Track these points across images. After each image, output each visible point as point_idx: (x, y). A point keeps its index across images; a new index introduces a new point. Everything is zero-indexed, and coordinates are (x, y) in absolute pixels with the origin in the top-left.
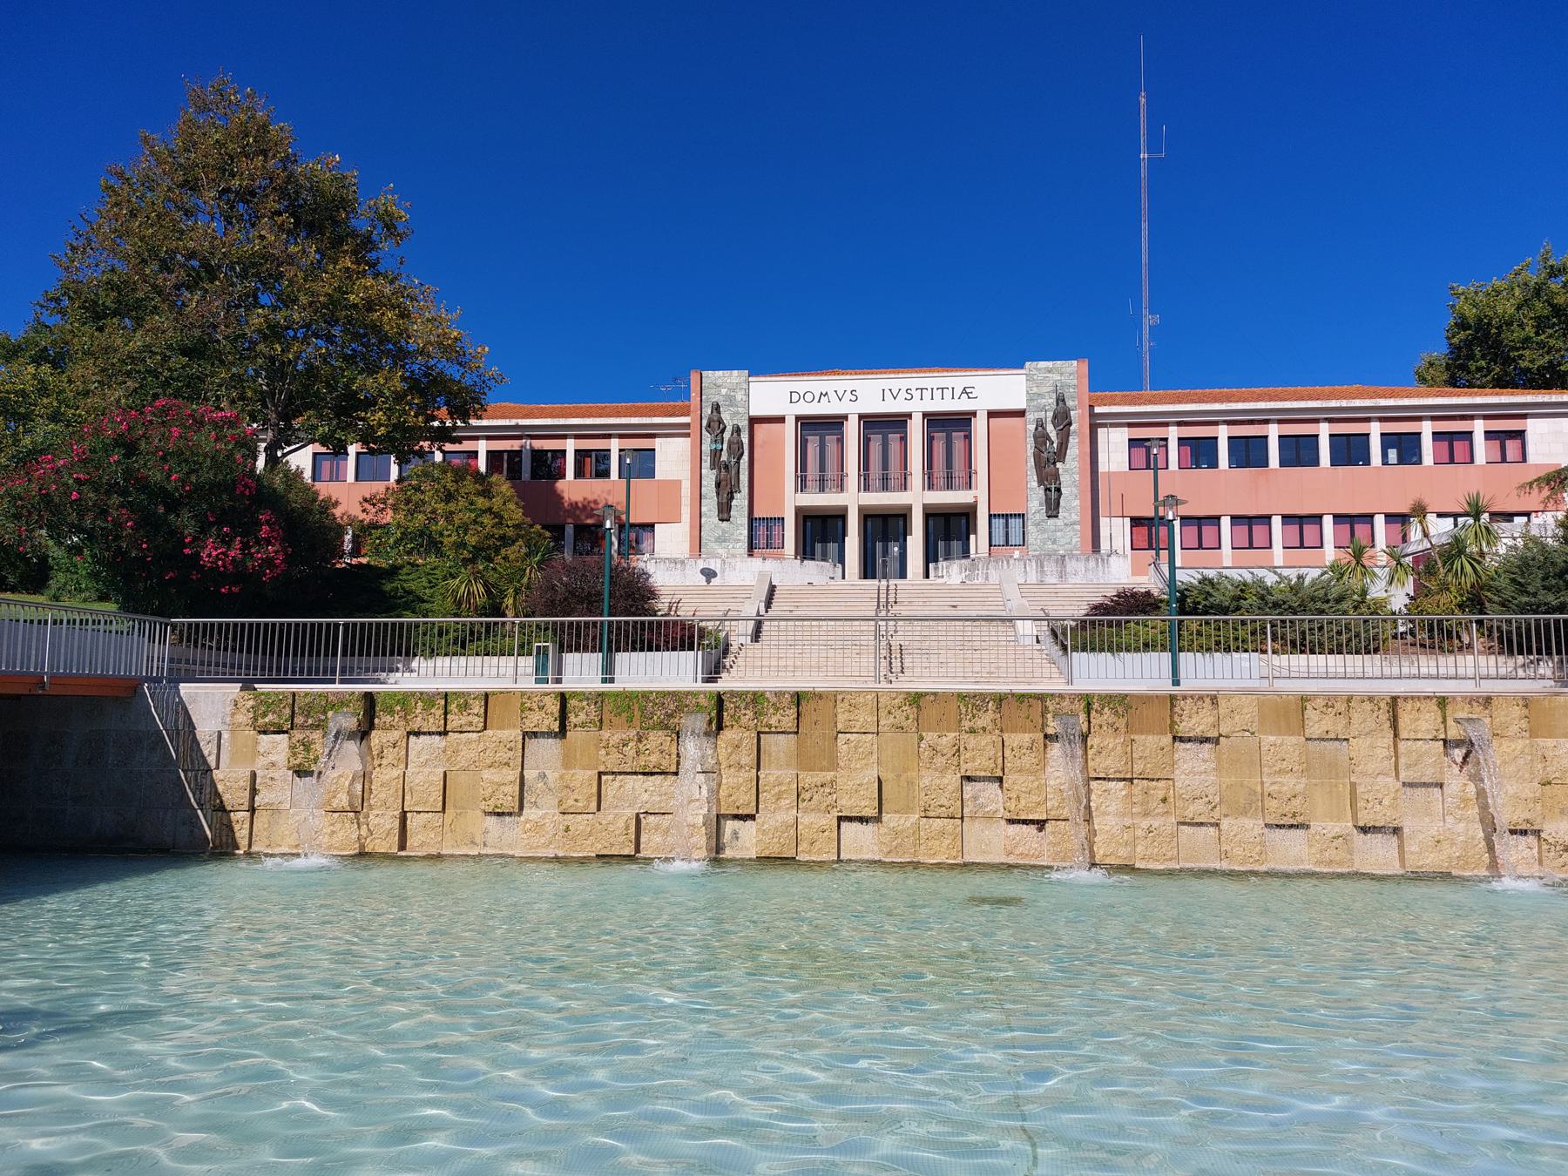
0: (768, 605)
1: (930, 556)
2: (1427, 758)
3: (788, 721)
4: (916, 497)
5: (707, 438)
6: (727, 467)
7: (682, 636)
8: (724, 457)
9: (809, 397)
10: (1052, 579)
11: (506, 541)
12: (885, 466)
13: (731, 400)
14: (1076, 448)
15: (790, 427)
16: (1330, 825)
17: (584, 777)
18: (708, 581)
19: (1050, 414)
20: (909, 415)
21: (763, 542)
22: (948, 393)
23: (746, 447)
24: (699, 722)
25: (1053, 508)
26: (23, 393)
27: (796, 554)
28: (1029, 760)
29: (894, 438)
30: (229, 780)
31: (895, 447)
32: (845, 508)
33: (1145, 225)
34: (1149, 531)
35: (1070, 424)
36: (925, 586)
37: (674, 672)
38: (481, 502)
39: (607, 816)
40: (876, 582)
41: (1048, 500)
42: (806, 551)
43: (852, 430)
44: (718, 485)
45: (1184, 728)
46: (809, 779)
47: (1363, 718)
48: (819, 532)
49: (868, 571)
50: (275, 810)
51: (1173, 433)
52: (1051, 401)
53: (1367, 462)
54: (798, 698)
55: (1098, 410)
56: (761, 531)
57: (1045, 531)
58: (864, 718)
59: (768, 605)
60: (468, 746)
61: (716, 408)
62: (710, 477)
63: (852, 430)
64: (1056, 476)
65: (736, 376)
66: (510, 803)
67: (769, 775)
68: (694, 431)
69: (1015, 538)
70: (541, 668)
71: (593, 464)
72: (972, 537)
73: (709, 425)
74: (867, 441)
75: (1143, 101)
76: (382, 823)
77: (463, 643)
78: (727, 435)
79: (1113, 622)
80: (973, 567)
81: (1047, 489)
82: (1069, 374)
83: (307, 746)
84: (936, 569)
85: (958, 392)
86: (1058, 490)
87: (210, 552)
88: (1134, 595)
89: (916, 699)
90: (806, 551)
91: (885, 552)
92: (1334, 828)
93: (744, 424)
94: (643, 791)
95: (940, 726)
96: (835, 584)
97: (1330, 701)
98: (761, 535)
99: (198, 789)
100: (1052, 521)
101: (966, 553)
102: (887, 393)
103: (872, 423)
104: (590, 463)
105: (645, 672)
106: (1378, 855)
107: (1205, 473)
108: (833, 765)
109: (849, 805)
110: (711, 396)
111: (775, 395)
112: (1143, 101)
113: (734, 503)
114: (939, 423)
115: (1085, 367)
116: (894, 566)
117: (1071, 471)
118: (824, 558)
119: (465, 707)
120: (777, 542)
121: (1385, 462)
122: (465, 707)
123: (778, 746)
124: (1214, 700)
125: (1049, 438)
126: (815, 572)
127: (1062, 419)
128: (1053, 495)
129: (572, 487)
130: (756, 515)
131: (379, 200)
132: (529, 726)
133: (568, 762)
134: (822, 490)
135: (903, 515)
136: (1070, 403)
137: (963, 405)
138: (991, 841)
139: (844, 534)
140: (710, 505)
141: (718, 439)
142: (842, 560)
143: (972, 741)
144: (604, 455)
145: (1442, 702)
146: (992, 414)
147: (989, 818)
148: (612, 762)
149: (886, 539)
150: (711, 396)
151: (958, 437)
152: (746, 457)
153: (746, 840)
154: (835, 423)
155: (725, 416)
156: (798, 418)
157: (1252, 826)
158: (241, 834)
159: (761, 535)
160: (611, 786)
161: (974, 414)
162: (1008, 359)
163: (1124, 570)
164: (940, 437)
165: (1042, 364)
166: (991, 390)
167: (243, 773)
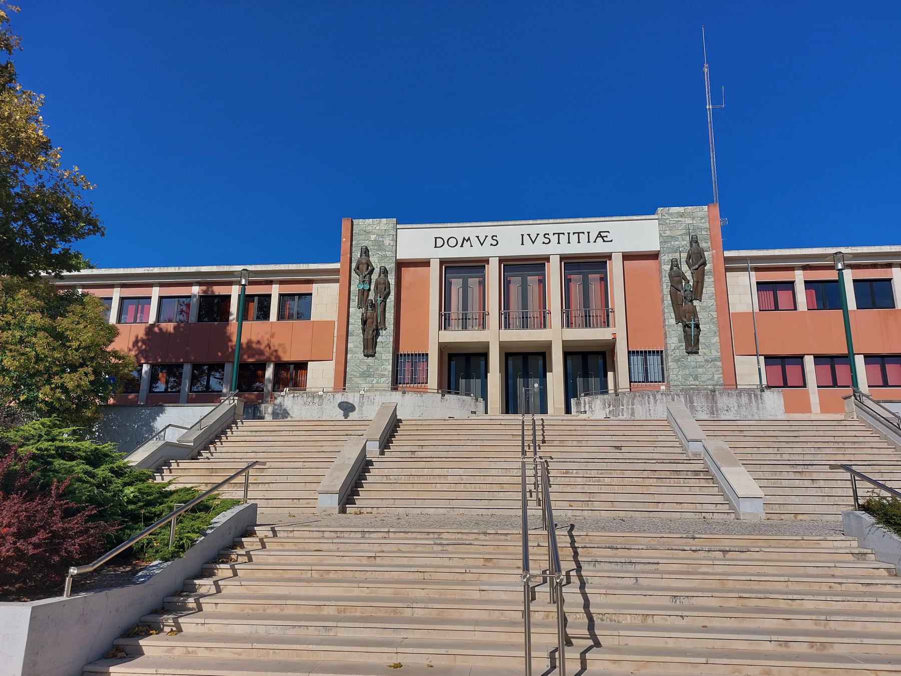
1: (570, 392)
4: (556, 335)
5: (356, 278)
6: (373, 306)
8: (372, 296)
9: (452, 242)
12: (525, 305)
13: (380, 245)
15: (434, 269)
18: (346, 416)
19: (684, 255)
20: (547, 259)
21: (408, 376)
22: (583, 238)
23: (392, 287)
25: (692, 345)
27: (440, 386)
29: (594, 278)
31: (595, 287)
32: (486, 345)
35: (704, 264)
36: (579, 425)
40: (519, 417)
41: (687, 337)
42: (448, 386)
43: (493, 272)
44: (364, 322)
48: (462, 368)
49: (510, 405)
52: (685, 242)
57: (685, 367)
61: (366, 252)
62: (356, 314)
63: (493, 272)
64: (694, 313)
72: (610, 375)
73: (358, 267)
78: (375, 276)
81: (686, 326)
82: (701, 219)
84: (578, 404)
85: (593, 237)
86: (697, 326)
90: (448, 386)
91: (526, 385)
93: (391, 266)
96: (478, 416)
100: (691, 358)
102: (526, 238)
103: (510, 265)
104: (131, 308)
111: (417, 241)
113: (379, 339)
114: (574, 264)
116: (535, 401)
117: (706, 309)
120: (421, 376)
125: (685, 278)
126: (456, 406)
127: (697, 259)
130: (401, 351)
134: (465, 328)
136: (703, 245)
137: (599, 248)
139: (487, 371)
140: (356, 342)
144: (837, 285)
146: (627, 257)
149: (526, 375)
150: (360, 241)
152: (392, 297)
154: (477, 266)
155: (374, 260)
156: (442, 262)
159: (405, 372)
162: (645, 208)
164: (576, 278)
165: (674, 210)
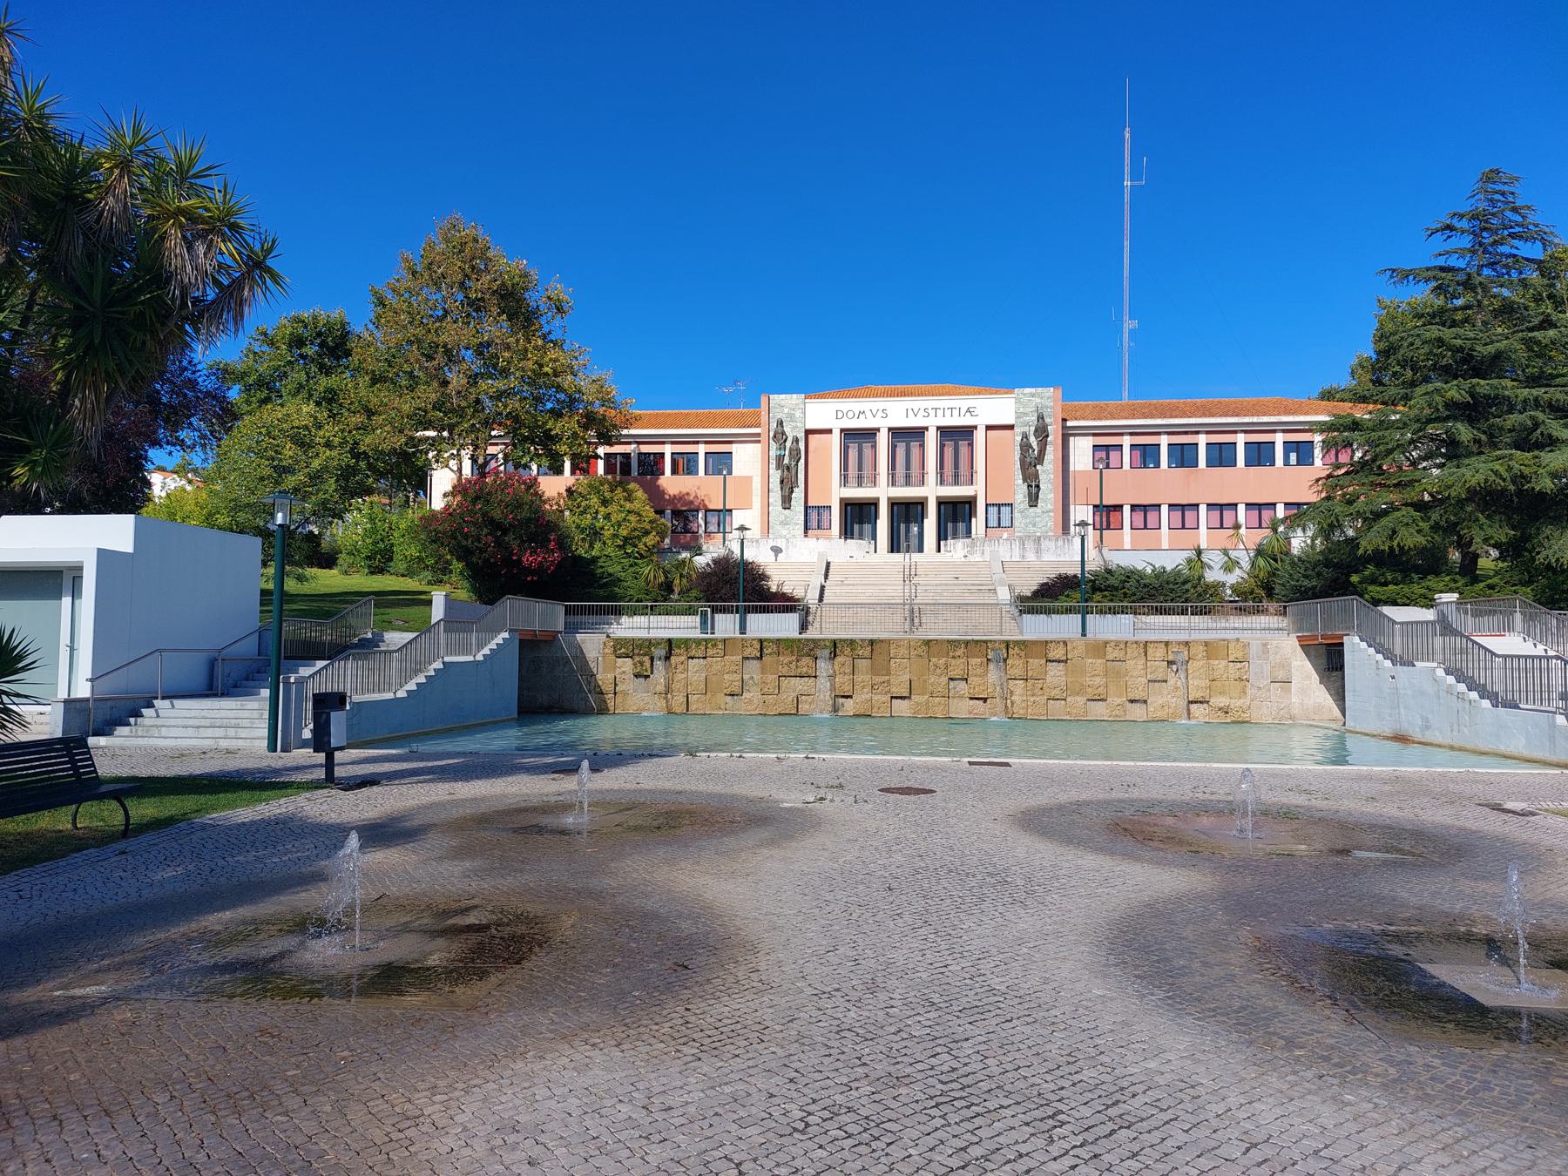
0: (826, 577)
1: (942, 536)
2: (1160, 670)
3: (867, 653)
4: (931, 491)
7: (784, 603)
8: (786, 461)
10: (1031, 556)
11: (647, 533)
13: (791, 417)
14: (1053, 454)
15: (836, 437)
16: (1115, 700)
17: (771, 678)
22: (956, 412)
24: (826, 652)
25: (1033, 500)
26: (306, 427)
28: (979, 671)
29: (915, 445)
30: (604, 678)
31: (915, 451)
33: (1127, 243)
36: (942, 562)
37: (783, 626)
38: (628, 506)
40: (901, 555)
41: (1030, 494)
42: (847, 533)
45: (1051, 656)
48: (857, 516)
49: (894, 547)
50: (625, 694)
51: (1126, 441)
53: (1273, 464)
54: (872, 642)
55: (1069, 424)
56: (814, 516)
58: (903, 651)
59: (826, 577)
60: (716, 663)
61: (781, 423)
62: (776, 476)
63: (883, 439)
64: (1037, 476)
65: (794, 399)
67: (858, 678)
68: (764, 438)
69: (1005, 521)
70: (704, 622)
71: (685, 465)
74: (894, 447)
75: (1127, 135)
78: (788, 444)
79: (1054, 594)
80: (973, 545)
83: (642, 663)
87: (527, 559)
88: (1067, 577)
89: (928, 643)
90: (847, 533)
91: (908, 530)
92: (1119, 701)
93: (801, 435)
94: (800, 685)
95: (939, 656)
97: (1117, 644)
98: (813, 520)
101: (968, 533)
103: (898, 434)
105: (765, 625)
106: (1137, 712)
107: (1150, 472)
108: (888, 674)
109: (896, 691)
110: (777, 414)
111: (826, 413)
112: (1127, 135)
115: (1059, 393)
116: (914, 542)
117: (1048, 472)
118: (861, 537)
119: (715, 645)
120: (825, 524)
121: (1287, 463)
122: (715, 645)
123: (863, 664)
124: (1065, 643)
127: (1042, 432)
128: (1034, 490)
129: (671, 483)
131: (546, 287)
132: (746, 654)
133: (763, 671)
134: (860, 485)
135: (921, 504)
136: (1047, 420)
137: (966, 421)
138: (962, 708)
140: (776, 497)
141: (782, 446)
142: (874, 537)
143: (953, 662)
145: (1167, 644)
146: (989, 428)
147: (962, 697)
148: (785, 671)
149: (908, 522)
150: (777, 414)
153: (849, 706)
154: (870, 434)
156: (842, 430)
157: (1081, 700)
158: (611, 704)
159: (813, 520)
160: (785, 682)
161: (975, 427)
163: (1063, 558)
165: (1027, 390)
166: (987, 408)
167: (610, 676)
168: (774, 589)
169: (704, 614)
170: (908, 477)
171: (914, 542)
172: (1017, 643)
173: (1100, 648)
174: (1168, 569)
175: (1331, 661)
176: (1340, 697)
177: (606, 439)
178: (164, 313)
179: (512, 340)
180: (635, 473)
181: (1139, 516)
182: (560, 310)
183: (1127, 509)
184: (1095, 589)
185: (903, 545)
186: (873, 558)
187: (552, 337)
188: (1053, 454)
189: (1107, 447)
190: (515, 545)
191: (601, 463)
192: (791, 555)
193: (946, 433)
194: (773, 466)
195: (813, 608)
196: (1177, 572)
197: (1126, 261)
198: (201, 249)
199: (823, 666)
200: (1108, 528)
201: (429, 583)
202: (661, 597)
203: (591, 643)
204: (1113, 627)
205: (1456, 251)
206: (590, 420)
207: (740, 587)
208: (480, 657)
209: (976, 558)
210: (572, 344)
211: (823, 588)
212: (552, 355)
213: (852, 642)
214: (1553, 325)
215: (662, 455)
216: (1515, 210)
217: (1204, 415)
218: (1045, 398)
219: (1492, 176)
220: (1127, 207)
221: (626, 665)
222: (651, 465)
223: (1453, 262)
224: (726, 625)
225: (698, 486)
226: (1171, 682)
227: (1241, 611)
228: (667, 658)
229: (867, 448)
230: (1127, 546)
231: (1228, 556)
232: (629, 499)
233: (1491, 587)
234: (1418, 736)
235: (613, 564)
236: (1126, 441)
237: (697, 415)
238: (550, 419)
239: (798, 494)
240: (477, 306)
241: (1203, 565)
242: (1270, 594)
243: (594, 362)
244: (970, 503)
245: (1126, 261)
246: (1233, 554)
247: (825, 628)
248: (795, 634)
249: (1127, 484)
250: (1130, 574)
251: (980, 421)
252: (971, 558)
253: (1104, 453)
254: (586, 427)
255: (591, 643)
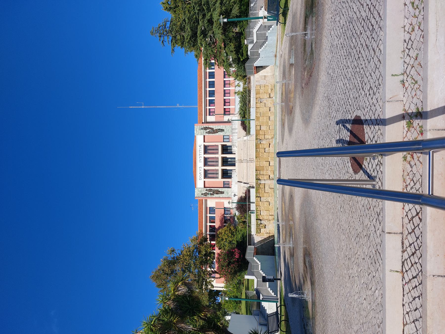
1: (231, 153)
2: (262, 104)
3: (259, 171)
4: (220, 156)
7: (248, 192)
8: (212, 193)
10: (237, 131)
11: (230, 229)
13: (201, 191)
14: (211, 126)
15: (206, 180)
16: (270, 115)
17: (265, 194)
21: (228, 185)
24: (259, 181)
25: (222, 130)
28: (263, 145)
30: (266, 236)
33: (158, 107)
34: (226, 112)
36: (238, 153)
37: (253, 192)
38: (223, 234)
39: (269, 192)
42: (230, 177)
43: (207, 168)
45: (259, 129)
46: (265, 169)
47: (258, 111)
48: (226, 174)
49: (234, 165)
54: (256, 170)
56: (226, 186)
58: (258, 163)
60: (262, 208)
61: (202, 194)
62: (215, 195)
63: (207, 168)
66: (268, 203)
67: (265, 174)
70: (253, 213)
71: (212, 220)
76: (271, 218)
77: (250, 227)
78: (207, 192)
79: (245, 127)
80: (234, 145)
87: (237, 256)
89: (256, 157)
90: (230, 177)
91: (230, 162)
95: (259, 155)
98: (227, 186)
99: (267, 240)
101: (231, 146)
103: (205, 164)
105: (253, 198)
106: (272, 109)
107: (216, 102)
110: (200, 195)
111: (200, 183)
116: (233, 160)
117: (215, 127)
118: (231, 173)
120: (228, 183)
123: (261, 173)
126: (234, 175)
127: (205, 128)
129: (217, 224)
131: (167, 254)
134: (218, 174)
140: (221, 195)
142: (231, 170)
146: (204, 142)
149: (228, 162)
150: (200, 195)
151: (208, 148)
154: (205, 171)
157: (269, 122)
160: (266, 191)
163: (237, 125)
165: (195, 132)
166: (200, 142)
167: (265, 234)
168: (244, 195)
169: (251, 213)
170: (216, 162)
171: (233, 160)
172: (256, 137)
173: (258, 118)
174: (239, 100)
175: (259, 68)
176: (267, 66)
177: (206, 240)
178: (190, 296)
179: (181, 262)
180: (214, 233)
181: (227, 104)
182: (173, 251)
183: (225, 107)
184: (244, 117)
185: (233, 163)
186: (237, 170)
187: (180, 253)
188: (211, 126)
189: (210, 112)
190: (233, 260)
191: (212, 242)
192: (236, 190)
193: (205, 152)
194: (213, 196)
195: (248, 185)
196: (240, 98)
197: (162, 107)
198: (180, 288)
199: (262, 182)
200: (229, 112)
201: (243, 286)
202: (246, 223)
203: (257, 238)
204: (253, 115)
205: (168, 39)
206: (201, 243)
207: (244, 204)
208: (260, 263)
209: (237, 145)
210: (182, 248)
211: (244, 183)
212: (184, 252)
213: (256, 175)
214: (185, 19)
215: (210, 226)
216: (159, 27)
217: (202, 89)
218: (197, 128)
219: (152, 33)
220: (151, 107)
221: (262, 230)
222: (212, 229)
223: (170, 40)
224: (253, 207)
225: (218, 216)
226: (265, 102)
227: (249, 82)
228: (261, 220)
229: (208, 172)
230: (234, 107)
231: (237, 86)
232: (222, 233)
233: (244, 30)
234: (275, 53)
235: (239, 236)
236: (208, 107)
237: (200, 216)
238: (201, 255)
239: (220, 190)
240: (173, 272)
241: (239, 92)
242: (245, 76)
243: (185, 242)
244: (223, 146)
245: (162, 107)
246: (236, 84)
247: (253, 182)
248: (255, 189)
249: (219, 107)
250: (241, 109)
251: (202, 144)
252: (237, 146)
253: (211, 113)
254: (203, 245)
255: (257, 238)
